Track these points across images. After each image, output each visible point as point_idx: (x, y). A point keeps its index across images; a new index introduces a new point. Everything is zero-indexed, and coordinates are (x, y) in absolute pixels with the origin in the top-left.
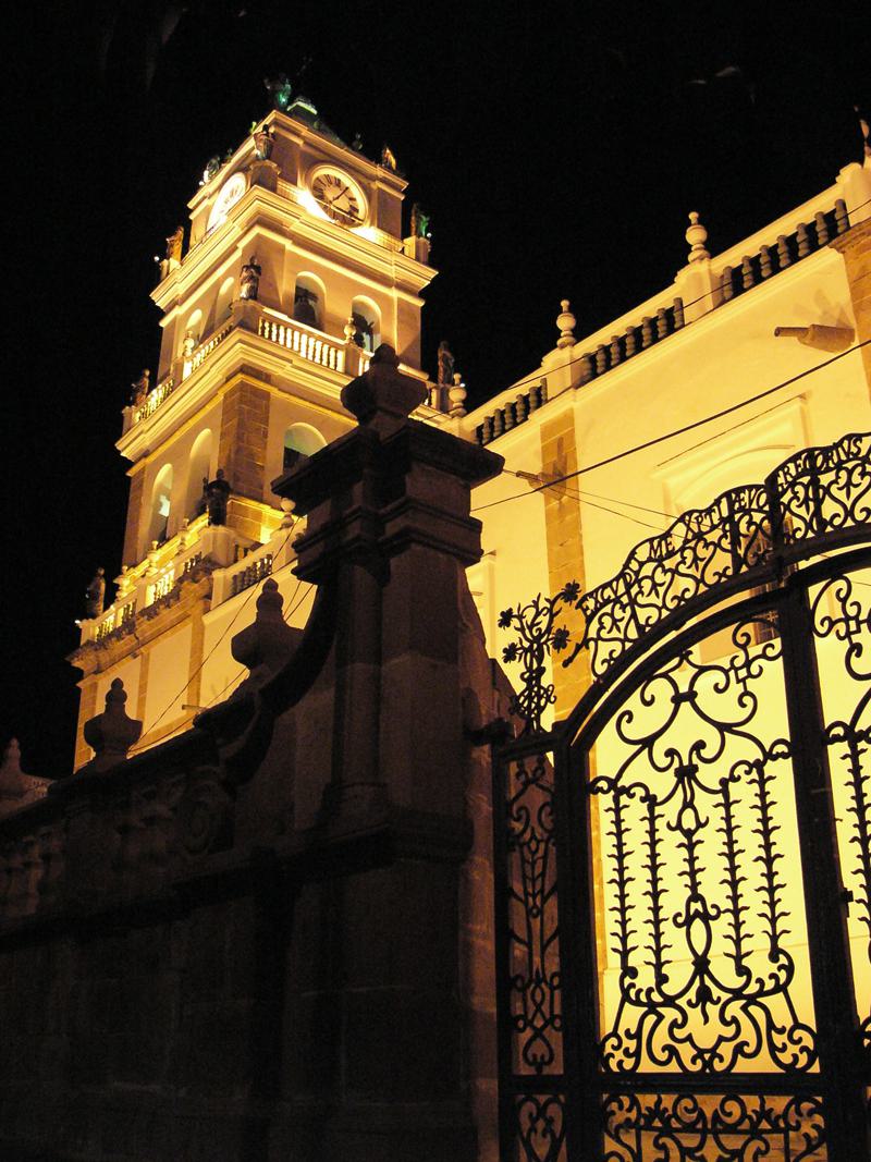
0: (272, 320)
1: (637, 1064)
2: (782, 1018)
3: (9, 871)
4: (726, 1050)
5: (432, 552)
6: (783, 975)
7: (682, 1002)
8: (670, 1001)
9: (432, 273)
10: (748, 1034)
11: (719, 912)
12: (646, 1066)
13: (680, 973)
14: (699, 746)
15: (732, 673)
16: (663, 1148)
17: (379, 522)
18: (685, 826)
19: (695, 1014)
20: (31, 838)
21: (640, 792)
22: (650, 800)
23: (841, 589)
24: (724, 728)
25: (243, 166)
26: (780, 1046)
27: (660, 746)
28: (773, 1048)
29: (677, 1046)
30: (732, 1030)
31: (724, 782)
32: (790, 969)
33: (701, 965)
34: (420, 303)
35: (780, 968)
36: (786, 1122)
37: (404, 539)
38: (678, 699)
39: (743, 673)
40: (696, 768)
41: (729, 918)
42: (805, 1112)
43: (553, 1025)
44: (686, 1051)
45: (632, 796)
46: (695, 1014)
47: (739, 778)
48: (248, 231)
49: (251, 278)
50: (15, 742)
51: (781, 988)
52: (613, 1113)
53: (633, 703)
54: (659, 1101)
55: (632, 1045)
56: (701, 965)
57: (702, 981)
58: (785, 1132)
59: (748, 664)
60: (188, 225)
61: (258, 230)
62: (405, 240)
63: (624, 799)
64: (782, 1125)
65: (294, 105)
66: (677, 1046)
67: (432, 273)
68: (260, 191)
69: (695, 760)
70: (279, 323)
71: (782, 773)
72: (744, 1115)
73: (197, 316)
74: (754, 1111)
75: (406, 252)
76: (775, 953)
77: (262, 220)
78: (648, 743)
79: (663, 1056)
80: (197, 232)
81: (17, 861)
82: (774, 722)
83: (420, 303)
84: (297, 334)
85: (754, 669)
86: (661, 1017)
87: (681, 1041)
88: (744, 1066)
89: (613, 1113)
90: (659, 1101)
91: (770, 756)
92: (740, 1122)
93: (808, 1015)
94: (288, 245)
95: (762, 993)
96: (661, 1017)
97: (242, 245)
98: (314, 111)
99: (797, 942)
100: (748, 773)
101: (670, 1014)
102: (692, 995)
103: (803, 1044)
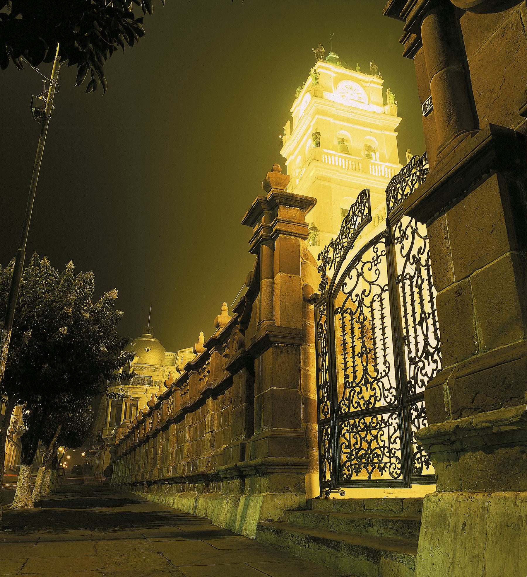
0: (328, 154)
1: (349, 410)
2: (387, 386)
3: (200, 380)
4: (372, 400)
5: (288, 237)
6: (387, 370)
7: (360, 385)
8: (357, 385)
9: (400, 119)
10: (378, 394)
11: (370, 351)
12: (352, 410)
13: (360, 374)
14: (364, 291)
15: (373, 263)
16: (356, 438)
17: (271, 229)
18: (361, 321)
19: (364, 388)
20: (205, 366)
21: (349, 311)
22: (352, 314)
23: (360, 222)
24: (371, 283)
25: (309, 90)
26: (386, 396)
27: (354, 294)
28: (385, 397)
29: (359, 400)
30: (374, 392)
31: (371, 303)
32: (389, 367)
33: (365, 370)
34: (396, 134)
35: (386, 367)
36: (389, 423)
37: (278, 232)
38: (358, 276)
39: (376, 262)
40: (363, 299)
41: (373, 351)
42: (393, 418)
43: (399, 437)
44: (362, 402)
45: (347, 313)
46: (364, 388)
47: (375, 300)
48: (314, 117)
49: (316, 138)
50: (202, 333)
51: (387, 375)
52: (343, 428)
53: (347, 280)
54: (355, 422)
55: (347, 402)
56: (365, 370)
57: (366, 376)
58: (388, 427)
59: (378, 257)
60: (291, 119)
61: (317, 116)
62: (385, 107)
63: (345, 315)
64: (388, 424)
65: (329, 56)
66: (359, 400)
67: (400, 119)
68: (316, 99)
69: (363, 297)
70: (331, 155)
71: (386, 295)
72: (378, 423)
73: (299, 158)
74: (380, 421)
75: (386, 113)
76: (385, 362)
77: (318, 112)
78: (350, 293)
79: (355, 405)
80: (295, 122)
81: (201, 377)
82: (384, 280)
83: (396, 134)
84: (333, 157)
85: (379, 261)
86: (355, 391)
87: (360, 399)
88: (378, 404)
89: (343, 428)
90: (355, 422)
91: (383, 290)
92: (376, 426)
93: (394, 385)
94: (331, 120)
95: (382, 377)
96: (355, 391)
97: (312, 124)
98: (338, 57)
99: (391, 359)
100: (378, 298)
101: (357, 389)
102: (363, 382)
103: (393, 394)
